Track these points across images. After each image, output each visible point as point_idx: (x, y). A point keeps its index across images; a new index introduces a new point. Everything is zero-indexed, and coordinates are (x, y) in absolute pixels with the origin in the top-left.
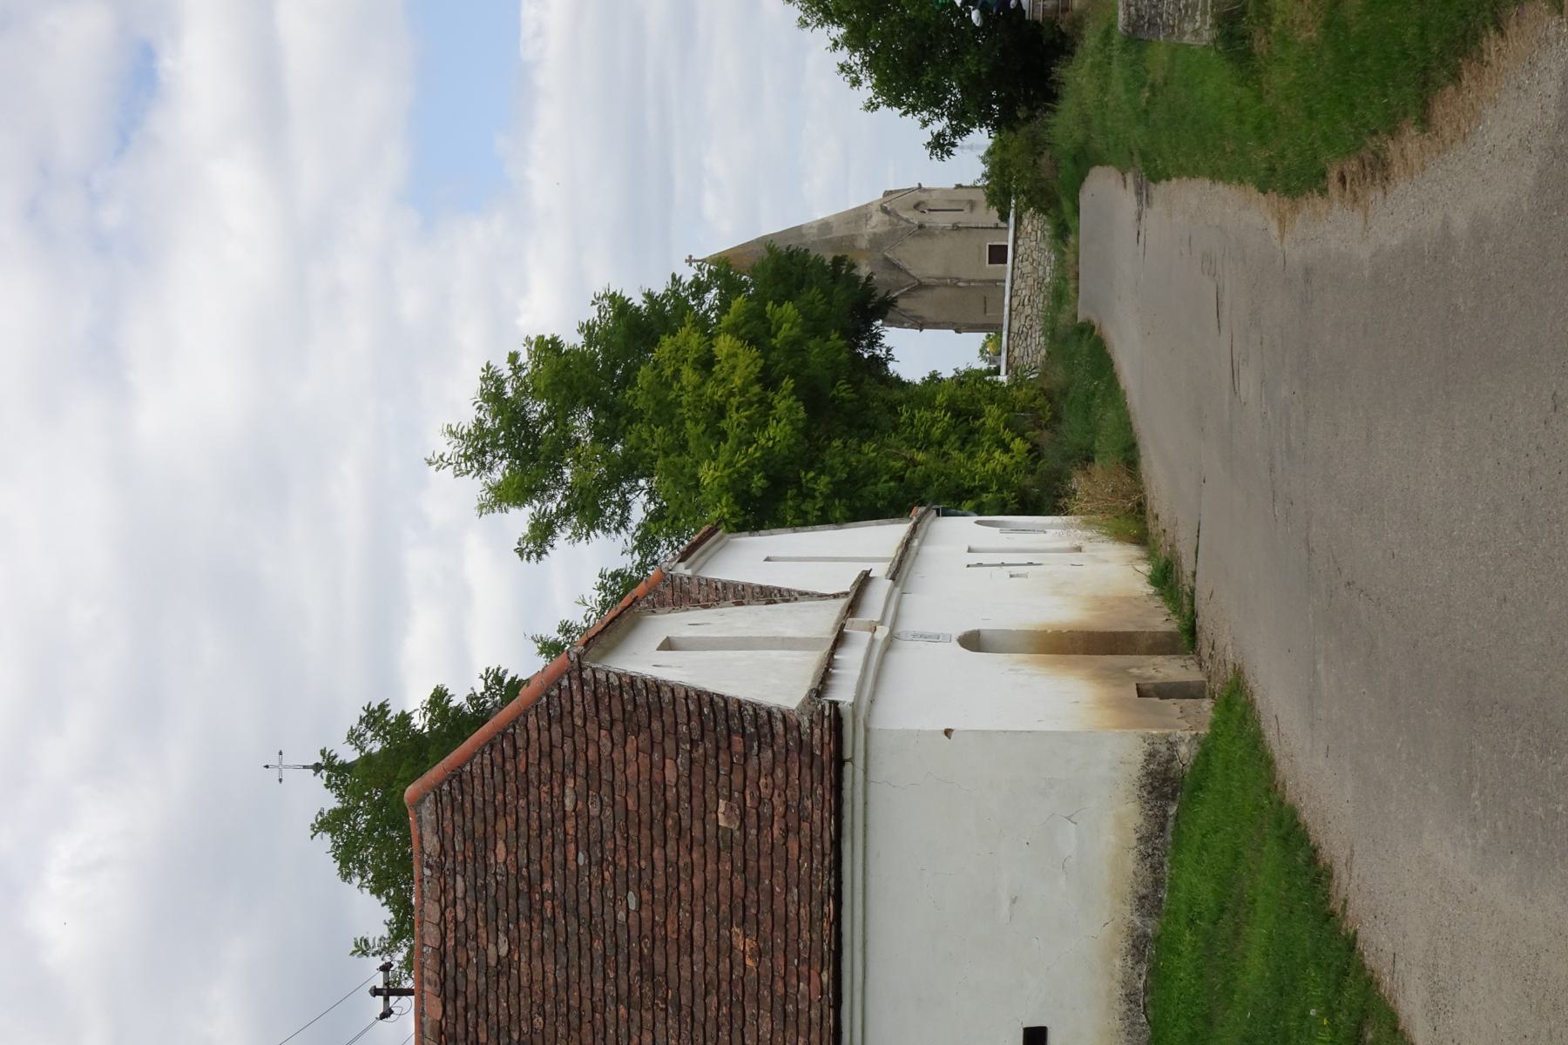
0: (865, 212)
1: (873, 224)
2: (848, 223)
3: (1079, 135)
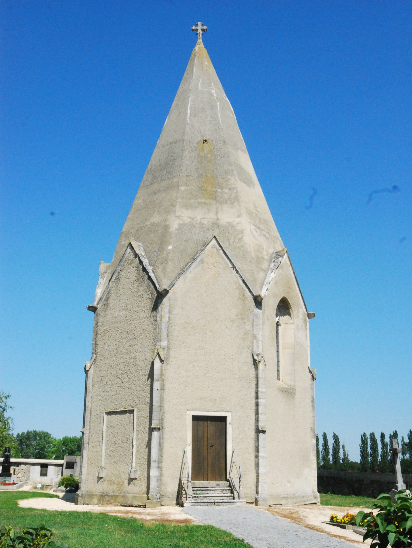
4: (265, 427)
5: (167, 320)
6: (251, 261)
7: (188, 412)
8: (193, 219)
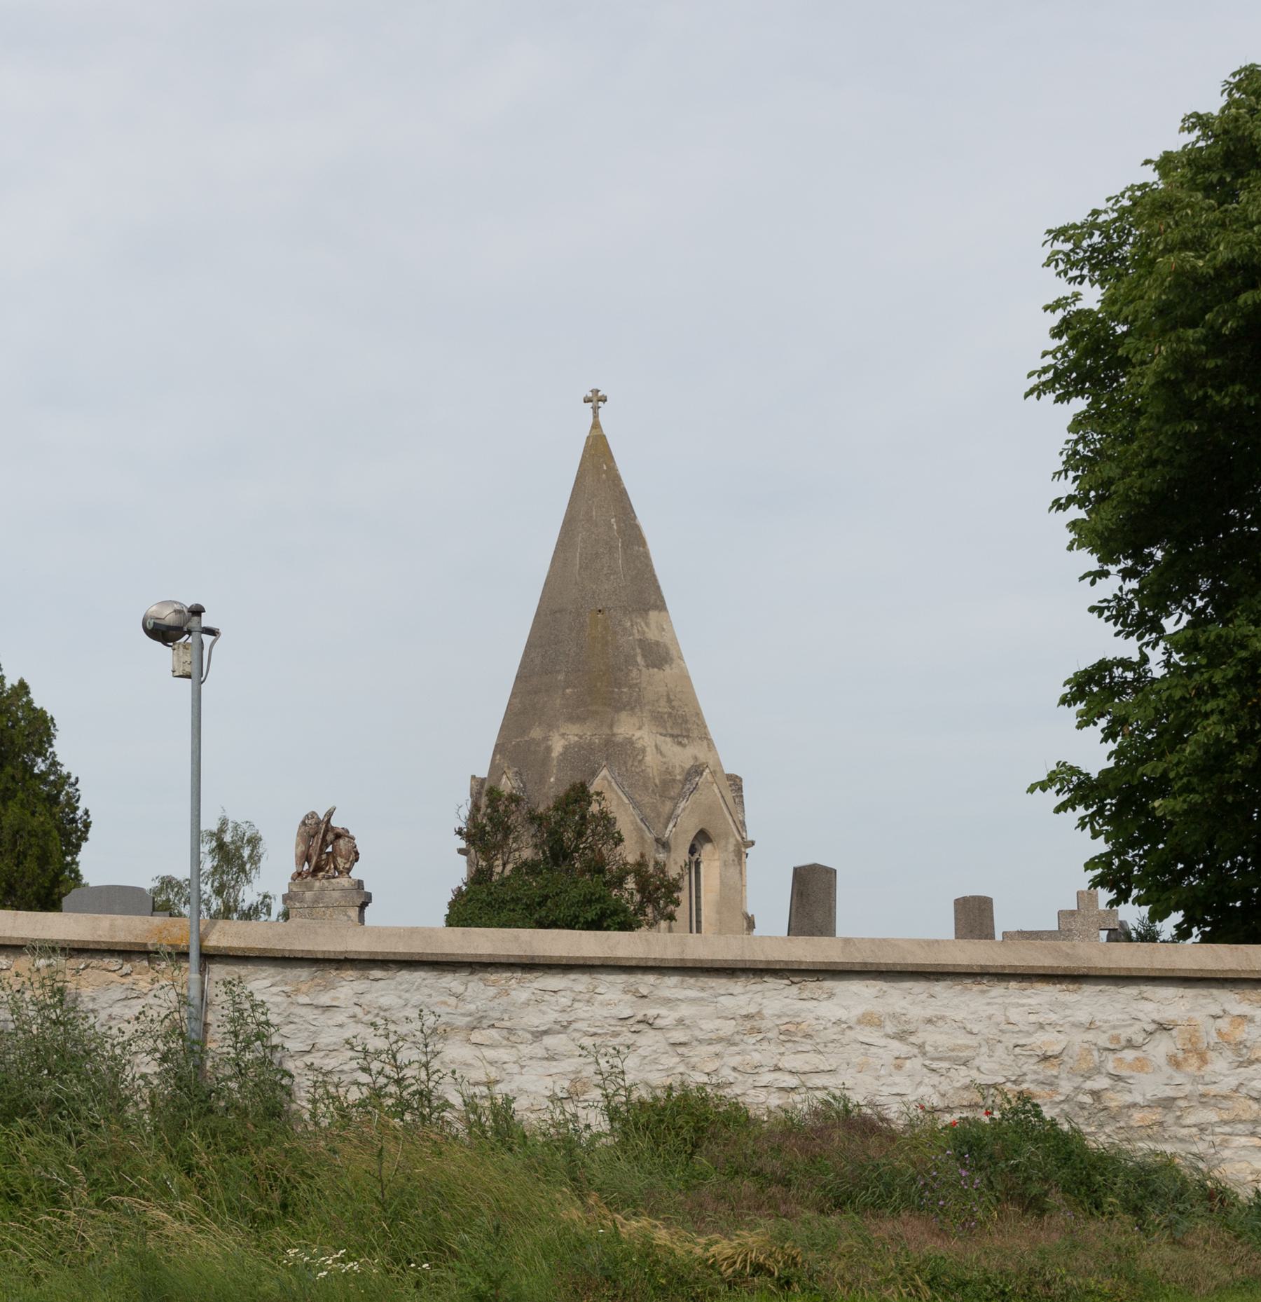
0: (695, 734)
1: (664, 748)
2: (669, 701)
6: (653, 791)
8: (581, 737)
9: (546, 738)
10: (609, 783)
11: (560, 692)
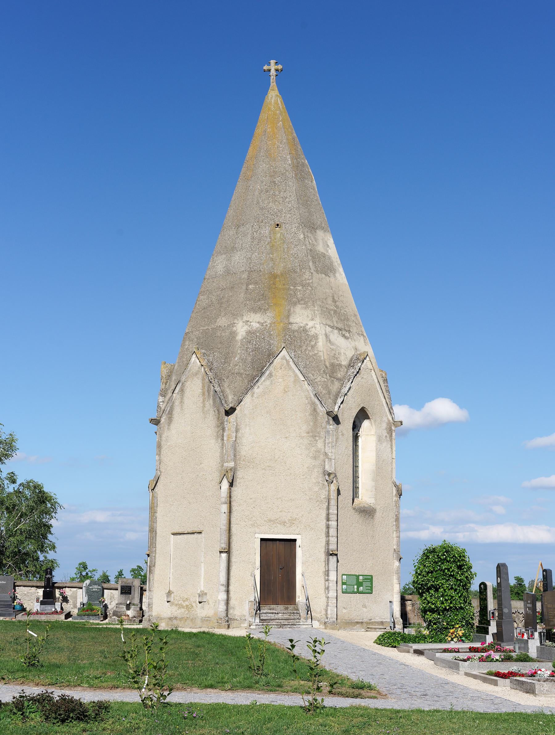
2: (334, 301)
3: (450, 707)
4: (52, 527)
5: (234, 439)
6: (324, 371)
7: (257, 535)
9: (233, 325)
10: (288, 362)
11: (244, 287)
